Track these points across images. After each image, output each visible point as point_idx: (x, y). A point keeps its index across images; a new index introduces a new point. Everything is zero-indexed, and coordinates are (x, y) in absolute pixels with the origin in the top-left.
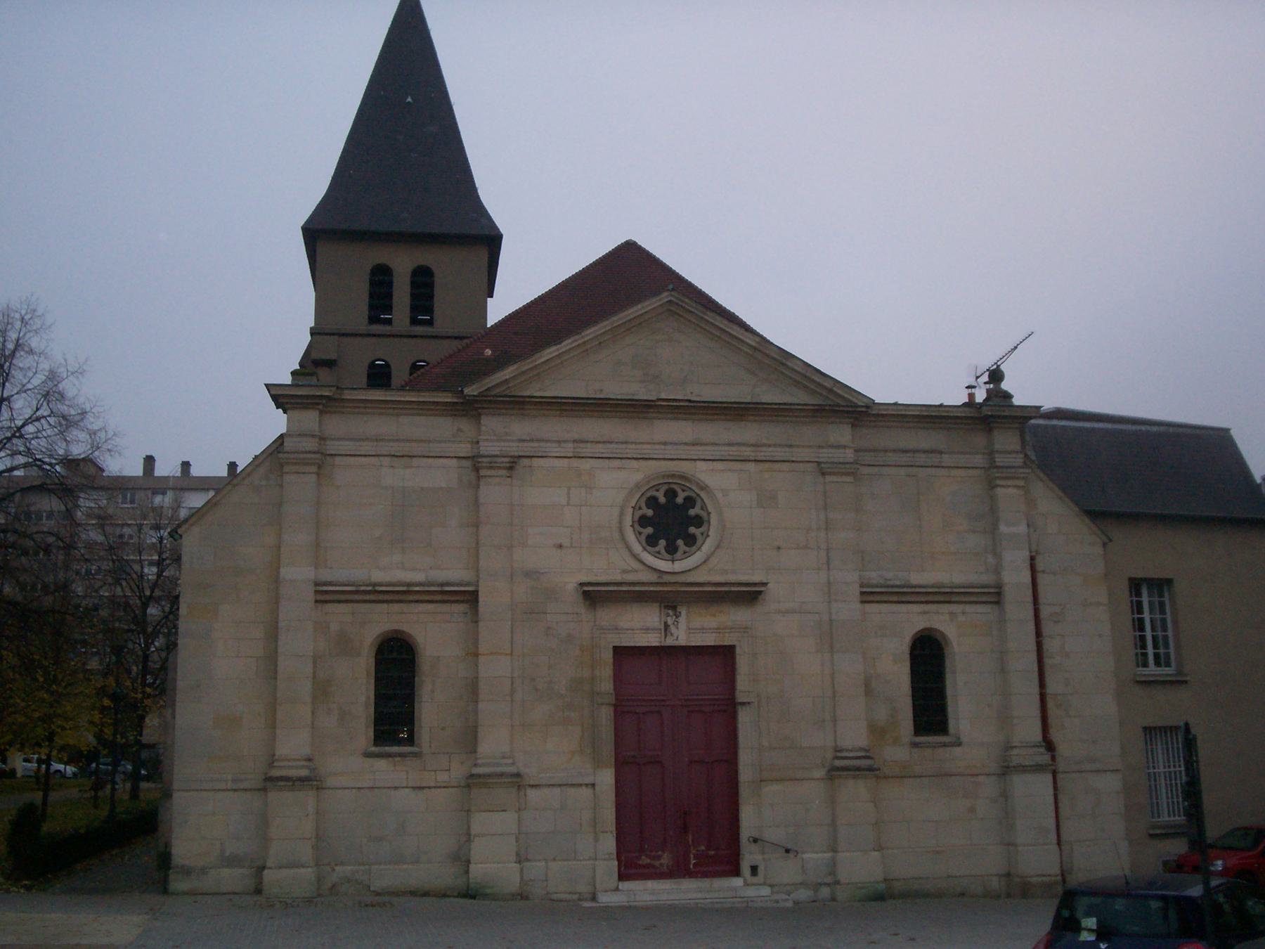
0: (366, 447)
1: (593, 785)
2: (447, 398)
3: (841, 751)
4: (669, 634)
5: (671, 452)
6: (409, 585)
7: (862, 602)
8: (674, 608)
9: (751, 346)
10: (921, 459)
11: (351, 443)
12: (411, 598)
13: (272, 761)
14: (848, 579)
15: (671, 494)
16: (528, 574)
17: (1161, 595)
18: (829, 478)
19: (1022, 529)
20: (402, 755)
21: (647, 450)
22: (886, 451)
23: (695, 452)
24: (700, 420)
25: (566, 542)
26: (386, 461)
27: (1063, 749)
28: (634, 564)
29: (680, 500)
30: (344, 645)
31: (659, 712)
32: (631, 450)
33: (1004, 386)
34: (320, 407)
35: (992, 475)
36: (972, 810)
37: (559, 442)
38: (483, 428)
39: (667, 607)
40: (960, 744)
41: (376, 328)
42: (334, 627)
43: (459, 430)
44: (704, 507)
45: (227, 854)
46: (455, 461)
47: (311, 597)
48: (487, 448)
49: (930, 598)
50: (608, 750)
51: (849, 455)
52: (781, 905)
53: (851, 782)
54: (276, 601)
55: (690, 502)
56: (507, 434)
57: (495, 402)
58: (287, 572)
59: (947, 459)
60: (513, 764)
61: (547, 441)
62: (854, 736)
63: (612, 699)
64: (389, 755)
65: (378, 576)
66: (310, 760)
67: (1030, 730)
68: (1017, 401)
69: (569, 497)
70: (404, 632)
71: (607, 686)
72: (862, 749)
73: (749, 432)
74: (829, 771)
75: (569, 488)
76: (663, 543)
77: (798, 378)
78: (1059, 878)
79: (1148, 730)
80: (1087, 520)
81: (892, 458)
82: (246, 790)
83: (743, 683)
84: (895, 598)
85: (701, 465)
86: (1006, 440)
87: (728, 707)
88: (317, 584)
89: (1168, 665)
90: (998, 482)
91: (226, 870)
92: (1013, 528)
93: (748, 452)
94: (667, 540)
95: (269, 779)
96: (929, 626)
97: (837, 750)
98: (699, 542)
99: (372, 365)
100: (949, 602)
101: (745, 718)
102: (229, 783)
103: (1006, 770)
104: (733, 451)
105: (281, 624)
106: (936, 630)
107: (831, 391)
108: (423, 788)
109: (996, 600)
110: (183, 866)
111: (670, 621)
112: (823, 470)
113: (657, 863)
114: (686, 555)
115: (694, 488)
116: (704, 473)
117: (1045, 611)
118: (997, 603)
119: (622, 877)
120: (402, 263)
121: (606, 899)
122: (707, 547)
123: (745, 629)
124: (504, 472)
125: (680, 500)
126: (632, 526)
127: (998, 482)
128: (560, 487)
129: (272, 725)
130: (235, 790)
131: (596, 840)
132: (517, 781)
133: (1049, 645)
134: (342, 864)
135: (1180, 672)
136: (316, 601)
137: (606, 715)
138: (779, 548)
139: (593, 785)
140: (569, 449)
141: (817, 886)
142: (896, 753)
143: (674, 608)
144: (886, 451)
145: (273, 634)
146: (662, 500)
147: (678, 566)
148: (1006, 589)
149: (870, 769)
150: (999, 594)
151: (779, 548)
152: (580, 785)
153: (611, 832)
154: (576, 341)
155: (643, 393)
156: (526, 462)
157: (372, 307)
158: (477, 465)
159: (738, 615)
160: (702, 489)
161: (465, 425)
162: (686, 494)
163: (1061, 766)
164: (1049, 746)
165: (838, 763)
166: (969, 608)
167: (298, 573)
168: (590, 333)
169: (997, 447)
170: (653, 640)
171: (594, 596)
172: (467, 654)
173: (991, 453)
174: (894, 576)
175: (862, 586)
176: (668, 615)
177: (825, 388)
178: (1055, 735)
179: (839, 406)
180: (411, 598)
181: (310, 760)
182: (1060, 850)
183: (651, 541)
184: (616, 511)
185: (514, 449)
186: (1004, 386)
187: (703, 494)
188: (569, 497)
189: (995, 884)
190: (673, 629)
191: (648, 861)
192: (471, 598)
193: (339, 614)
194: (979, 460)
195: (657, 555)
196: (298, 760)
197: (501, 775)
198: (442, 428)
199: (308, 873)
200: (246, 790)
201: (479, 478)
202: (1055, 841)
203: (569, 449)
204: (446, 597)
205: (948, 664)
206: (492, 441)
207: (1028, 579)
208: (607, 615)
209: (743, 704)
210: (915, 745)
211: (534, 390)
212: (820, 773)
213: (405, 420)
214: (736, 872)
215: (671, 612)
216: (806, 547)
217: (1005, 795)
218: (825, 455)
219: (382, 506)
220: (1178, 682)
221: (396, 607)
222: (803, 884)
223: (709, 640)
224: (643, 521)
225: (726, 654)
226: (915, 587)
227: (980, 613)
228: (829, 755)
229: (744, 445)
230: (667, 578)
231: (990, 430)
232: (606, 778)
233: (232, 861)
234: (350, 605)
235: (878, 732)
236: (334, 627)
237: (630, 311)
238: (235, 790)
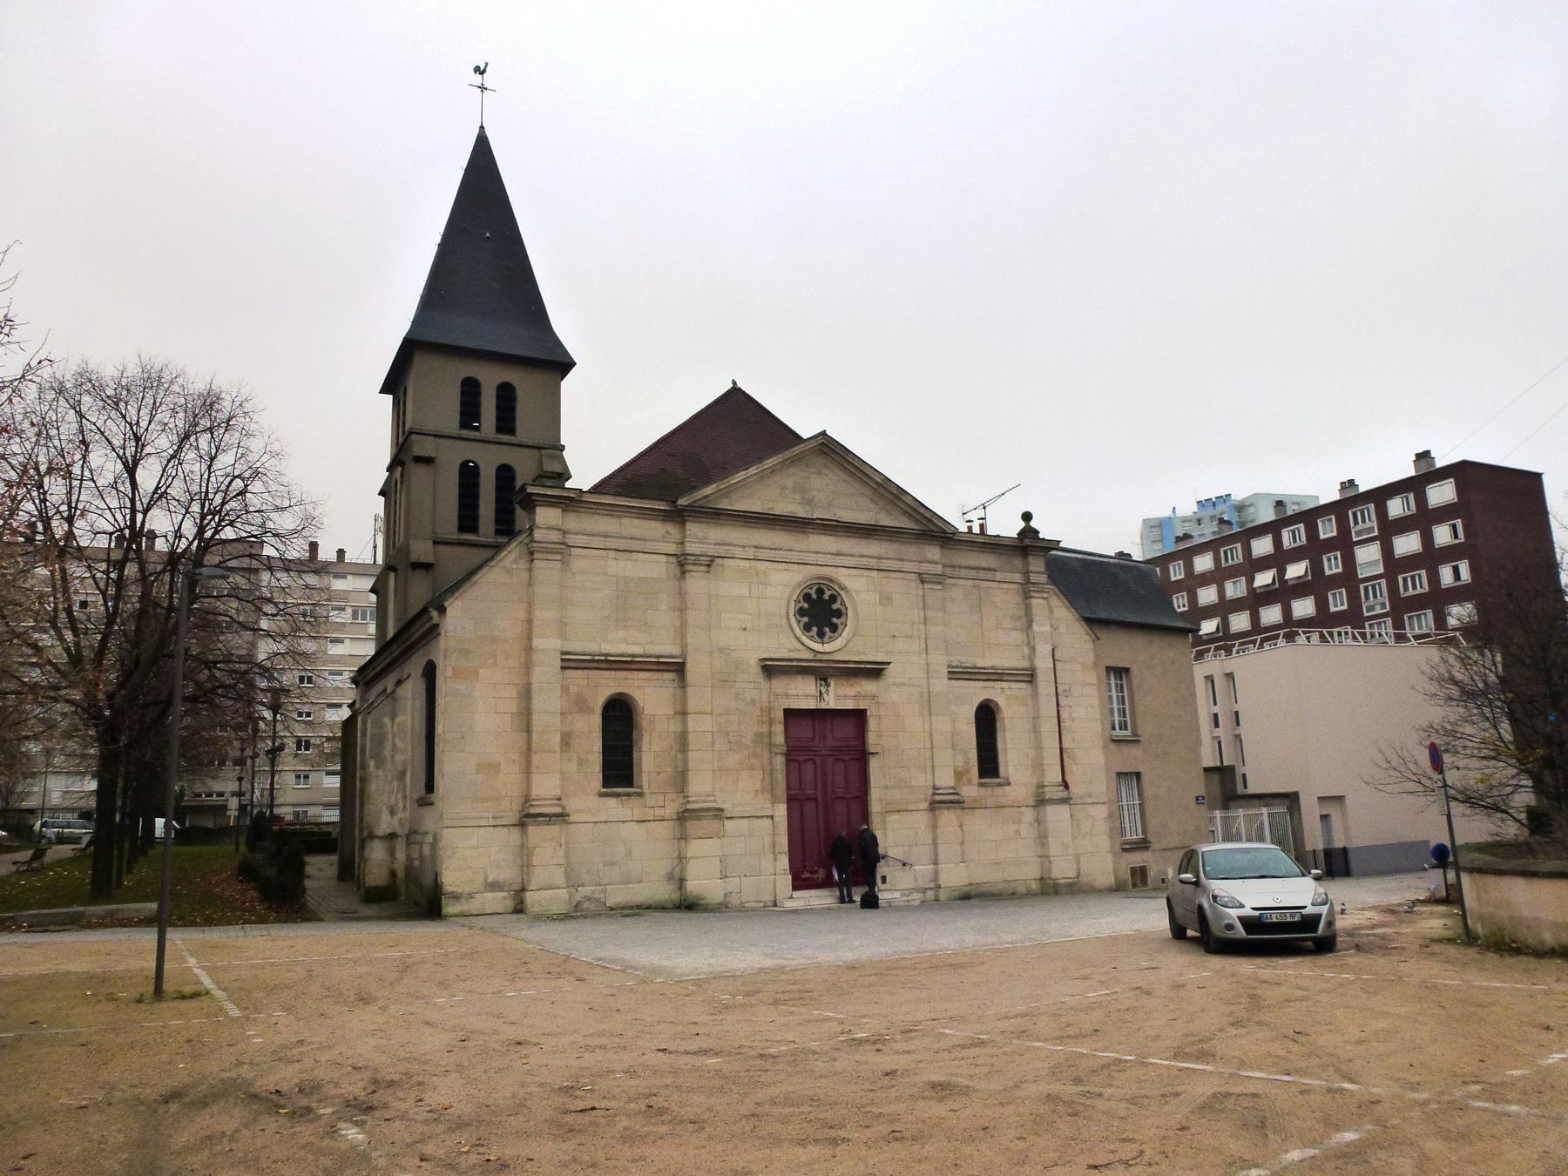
0: (597, 542)
1: (772, 817)
2: (662, 506)
3: (938, 789)
5: (822, 559)
6: (633, 656)
7: (950, 679)
8: (825, 680)
9: (877, 483)
10: (982, 574)
11: (586, 538)
13: (527, 799)
14: (940, 661)
15: (820, 592)
16: (721, 650)
17: (1121, 680)
18: (927, 586)
19: (1047, 628)
20: (628, 795)
21: (811, 558)
22: (960, 567)
23: (838, 560)
24: (840, 536)
25: (749, 626)
26: (612, 554)
28: (799, 646)
29: (826, 596)
30: (581, 704)
31: (814, 760)
32: (794, 557)
33: (1033, 524)
35: (1027, 590)
36: (1017, 832)
37: (744, 547)
38: (688, 532)
39: (821, 679)
40: (1009, 784)
41: (465, 433)
42: (573, 689)
43: (667, 532)
44: (843, 603)
45: (489, 881)
46: (664, 557)
47: (558, 664)
48: (691, 548)
49: (990, 677)
50: (781, 791)
51: (939, 569)
52: (912, 903)
53: (946, 812)
54: (528, 666)
55: (833, 598)
56: (705, 538)
57: (699, 512)
58: (538, 643)
59: (999, 576)
60: (715, 801)
61: (735, 546)
62: (946, 779)
63: (784, 750)
64: (618, 795)
65: (607, 648)
66: (559, 799)
67: (1054, 775)
68: (1041, 536)
71: (780, 739)
72: (951, 788)
73: (874, 547)
74: (930, 804)
77: (907, 509)
79: (1119, 774)
80: (1083, 623)
81: (963, 573)
82: (503, 826)
83: (872, 738)
84: (967, 676)
85: (843, 571)
86: (1037, 564)
87: (861, 756)
88: (563, 653)
89: (1126, 729)
90: (1033, 594)
91: (489, 894)
92: (1041, 627)
93: (873, 563)
95: (528, 815)
97: (935, 788)
98: (839, 631)
99: (464, 464)
100: (1001, 680)
101: (874, 764)
103: (1041, 802)
104: (864, 561)
105: (535, 686)
106: (992, 701)
107: (930, 520)
108: (644, 821)
110: (452, 893)
111: (823, 690)
112: (922, 579)
113: (814, 876)
114: (832, 639)
115: (836, 588)
116: (842, 576)
118: (1031, 682)
119: (795, 888)
120: (490, 378)
121: (790, 905)
122: (846, 633)
123: (874, 697)
124: (703, 568)
125: (826, 596)
127: (1033, 594)
129: (528, 772)
130: (495, 826)
131: (775, 860)
132: (719, 813)
133: (1064, 715)
134: (583, 885)
135: (1135, 734)
136: (562, 668)
137: (780, 762)
138: (894, 636)
139: (772, 817)
140: (750, 553)
141: (924, 890)
142: (970, 791)
143: (825, 680)
144: (960, 567)
145: (526, 694)
146: (814, 596)
147: (827, 648)
148: (1038, 671)
149: (959, 802)
150: (1032, 676)
151: (894, 636)
152: (763, 817)
155: (800, 511)
156: (719, 561)
157: (462, 414)
158: (683, 562)
159: (868, 686)
160: (842, 589)
161: (673, 530)
162: (830, 592)
164: (1066, 786)
165: (938, 798)
166: (1013, 685)
167: (548, 645)
168: (769, 463)
169: (1031, 568)
170: (811, 704)
171: (771, 669)
173: (1026, 573)
175: (949, 667)
176: (821, 685)
177: (926, 518)
178: (1068, 779)
179: (932, 531)
180: (633, 667)
181: (559, 799)
183: (807, 628)
184: (784, 603)
185: (712, 550)
186: (1033, 524)
187: (842, 593)
189: (1034, 886)
190: (825, 696)
191: (809, 875)
192: (679, 669)
193: (578, 678)
194: (1018, 577)
195: (811, 638)
196: (551, 799)
197: (709, 810)
198: (655, 529)
199: (563, 894)
200: (503, 826)
201: (683, 573)
203: (750, 553)
204: (661, 667)
205: (998, 725)
206: (696, 543)
208: (780, 684)
209: (873, 754)
210: (981, 785)
211: (724, 504)
212: (925, 805)
213: (626, 521)
216: (910, 637)
217: (1039, 821)
218: (925, 567)
220: (1134, 741)
221: (622, 674)
222: (916, 890)
223: (849, 705)
224: (801, 612)
225: (859, 716)
227: (1022, 689)
228: (930, 792)
229: (871, 557)
230: (819, 657)
231: (683, 522)
232: (781, 810)
233: (494, 886)
234: (586, 671)
235: (959, 775)
236: (573, 689)
237: (795, 449)
238: (495, 826)
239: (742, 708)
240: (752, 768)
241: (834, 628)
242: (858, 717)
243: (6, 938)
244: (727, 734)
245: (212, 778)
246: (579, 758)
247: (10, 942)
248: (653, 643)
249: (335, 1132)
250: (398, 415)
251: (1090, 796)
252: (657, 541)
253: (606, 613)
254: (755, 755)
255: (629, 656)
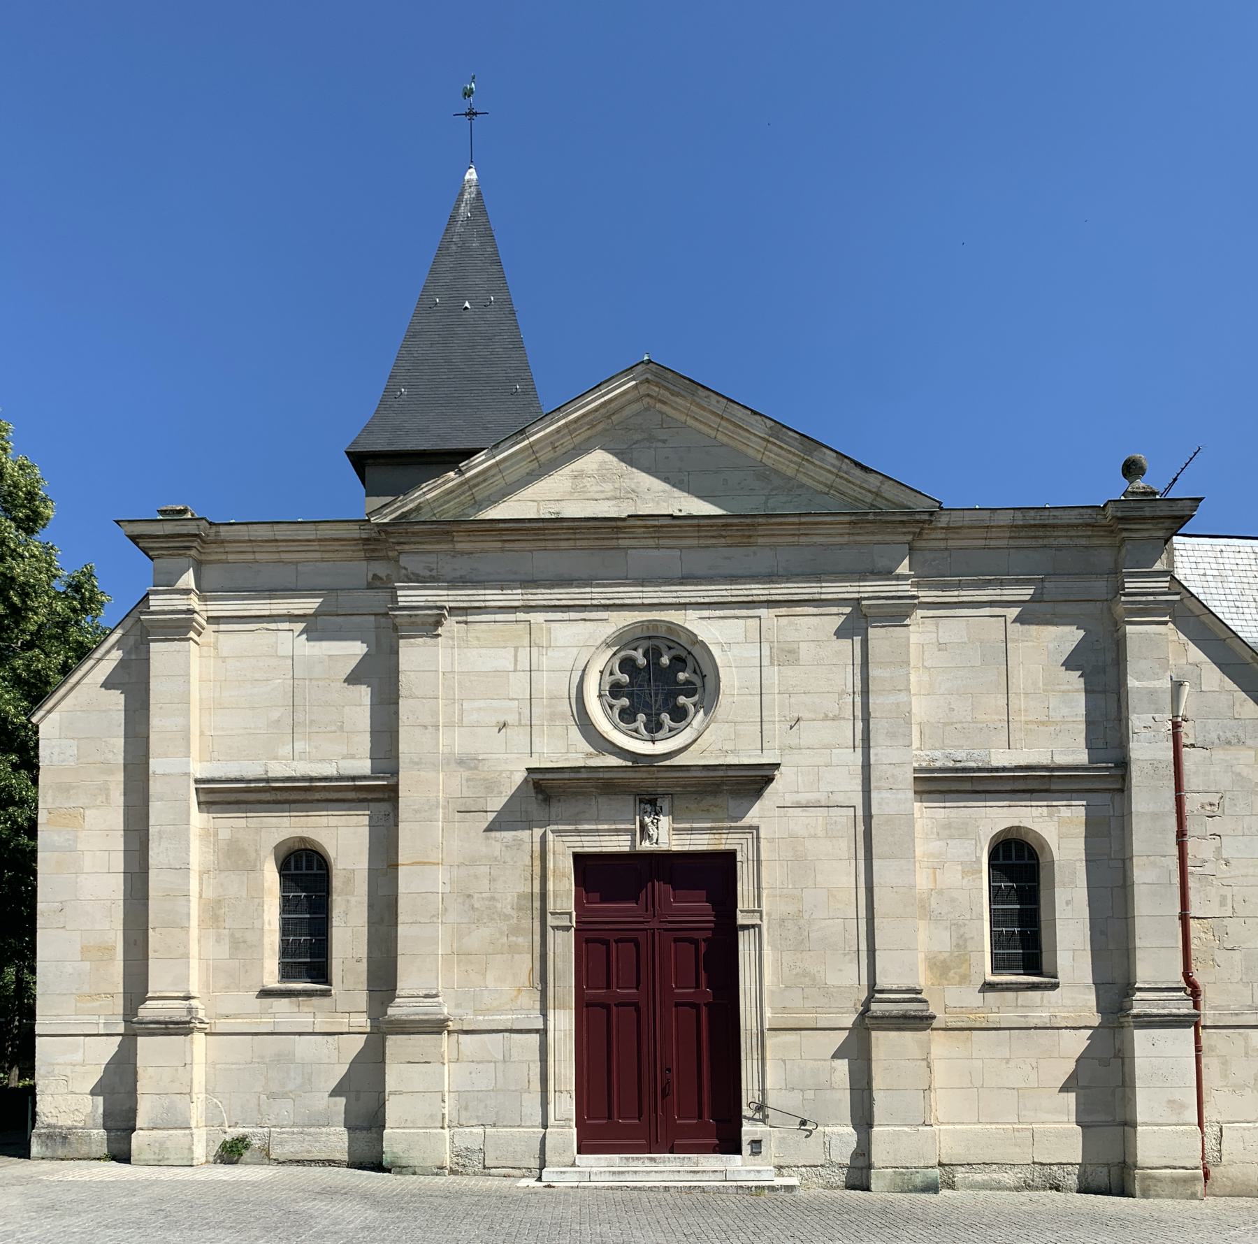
4: (645, 836)
8: (653, 802)
12: (317, 796)
15: (653, 654)
27: (1209, 996)
34: (193, 552)
46: (372, 618)
65: (278, 769)
69: (516, 660)
70: (313, 840)
75: (516, 649)
76: (641, 717)
78: (1201, 1172)
85: (692, 614)
94: (632, 704)
102: (101, 1026)
106: (1029, 830)
109: (1118, 786)
116: (691, 621)
117: (1192, 803)
143: (653, 802)
153: (568, 1092)
164: (1194, 991)
172: (388, 866)
174: (968, 754)
178: (1197, 977)
180: (317, 796)
182: (1202, 1132)
183: (627, 716)
188: (516, 660)
190: (652, 830)
202: (1196, 1121)
214: (738, 1151)
215: (648, 808)
219: (280, 681)
226: (997, 769)
239: (497, 853)
240: (513, 949)
241: (680, 715)
242: (727, 860)
244: (469, 896)
245: (1130, 1009)
246: (232, 935)
252: (452, 610)
253: (275, 715)
254: (515, 930)
255: (303, 779)
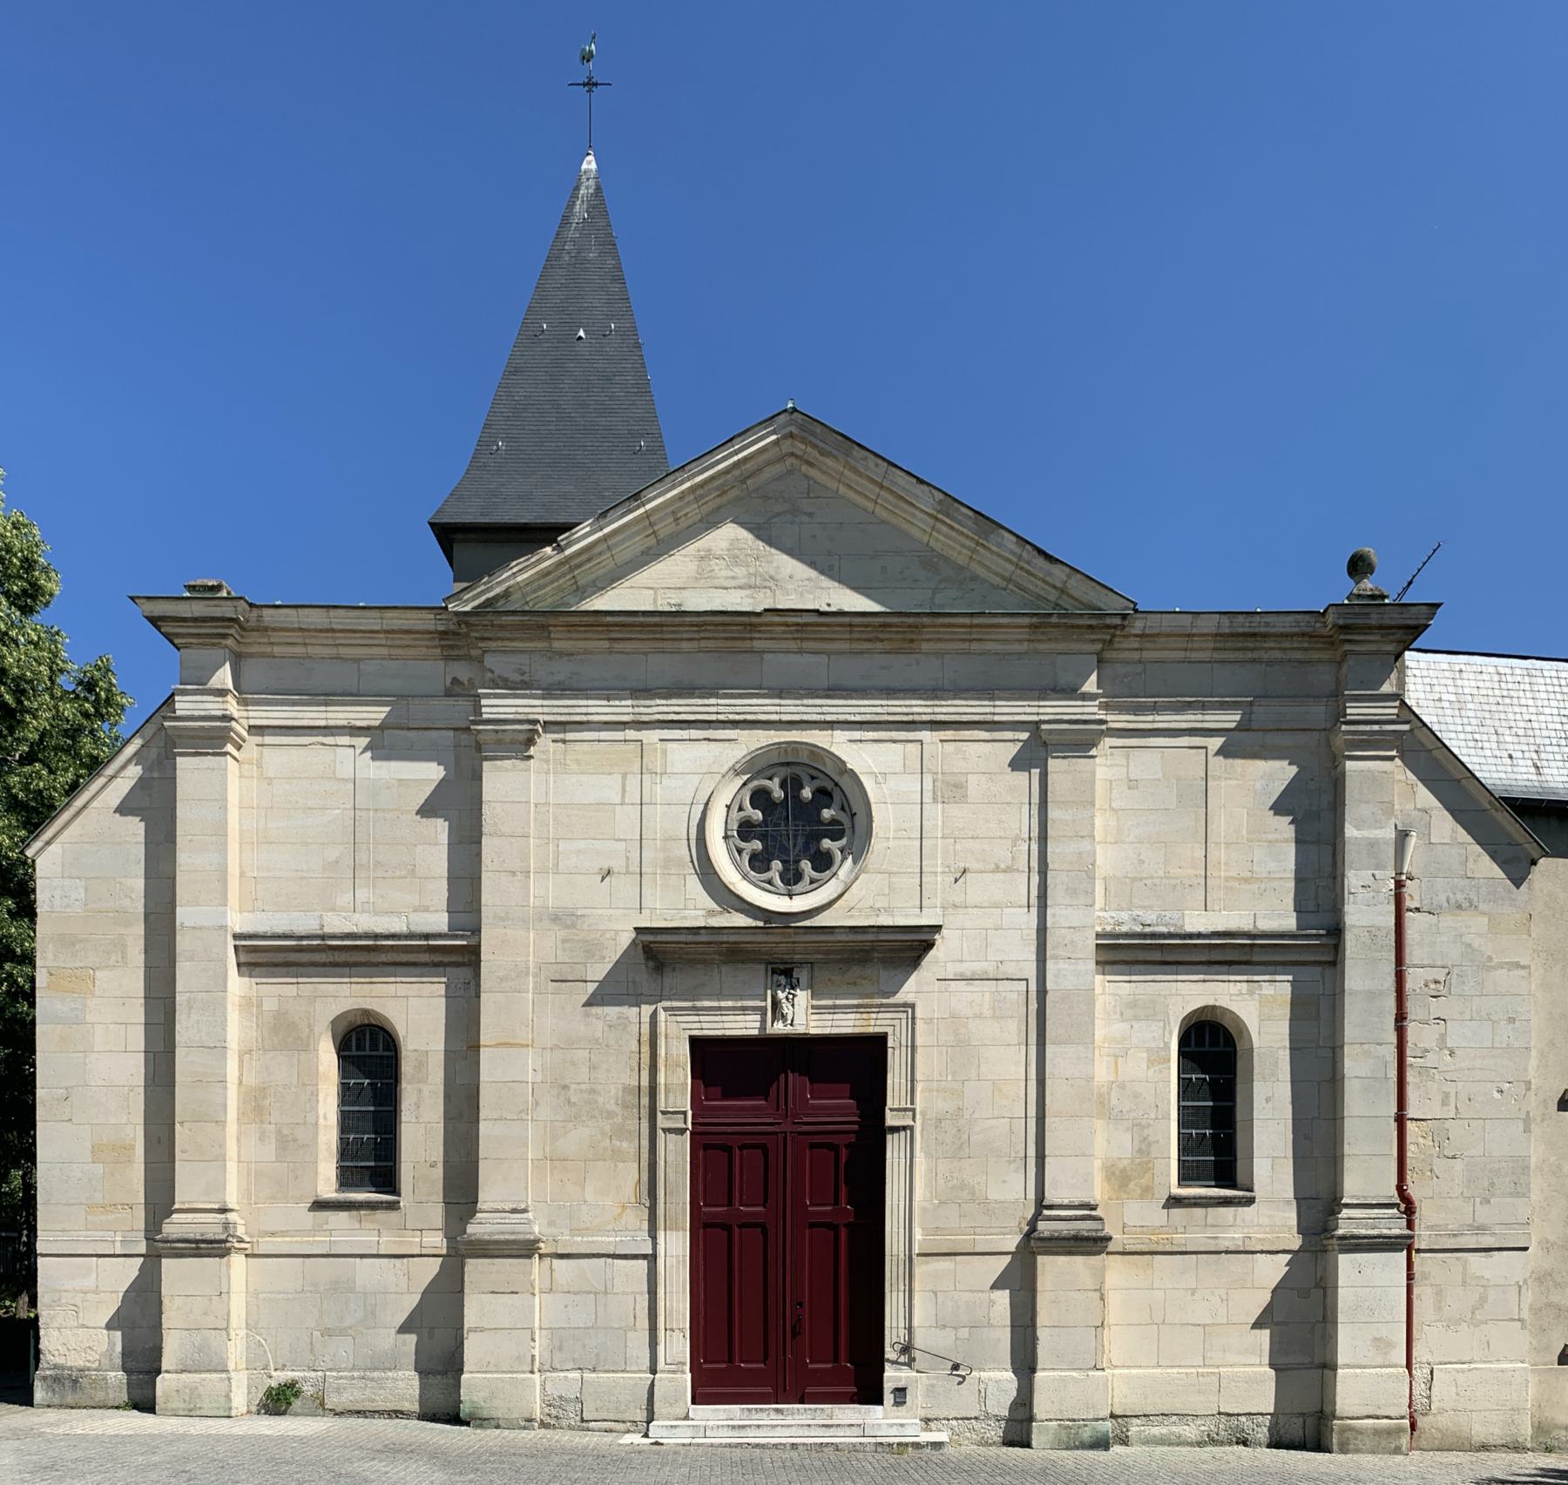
8: (788, 973)
12: (383, 958)
15: (792, 785)
27: (1426, 1214)
65: (336, 923)
78: (1407, 1422)
85: (840, 736)
96: (1211, 1003)
102: (118, 1244)
116: (838, 744)
126: (728, 807)
128: (610, 774)
143: (788, 973)
154: (631, 511)
163: (1423, 1238)
164: (1408, 1207)
178: (1413, 1191)
180: (383, 958)
183: (759, 863)
204: (437, 958)
207: (1391, 921)
214: (878, 1400)
215: (783, 980)
219: (337, 811)
226: (1191, 936)
235: (1120, 1178)
240: (617, 1155)
243: (1566, 1468)
244: (565, 1087)
247: (1563, 1466)
248: (426, 909)
249: (1326, 1251)
250: (356, 964)
251: (1481, 1229)
254: (619, 1132)
255: (367, 936)
